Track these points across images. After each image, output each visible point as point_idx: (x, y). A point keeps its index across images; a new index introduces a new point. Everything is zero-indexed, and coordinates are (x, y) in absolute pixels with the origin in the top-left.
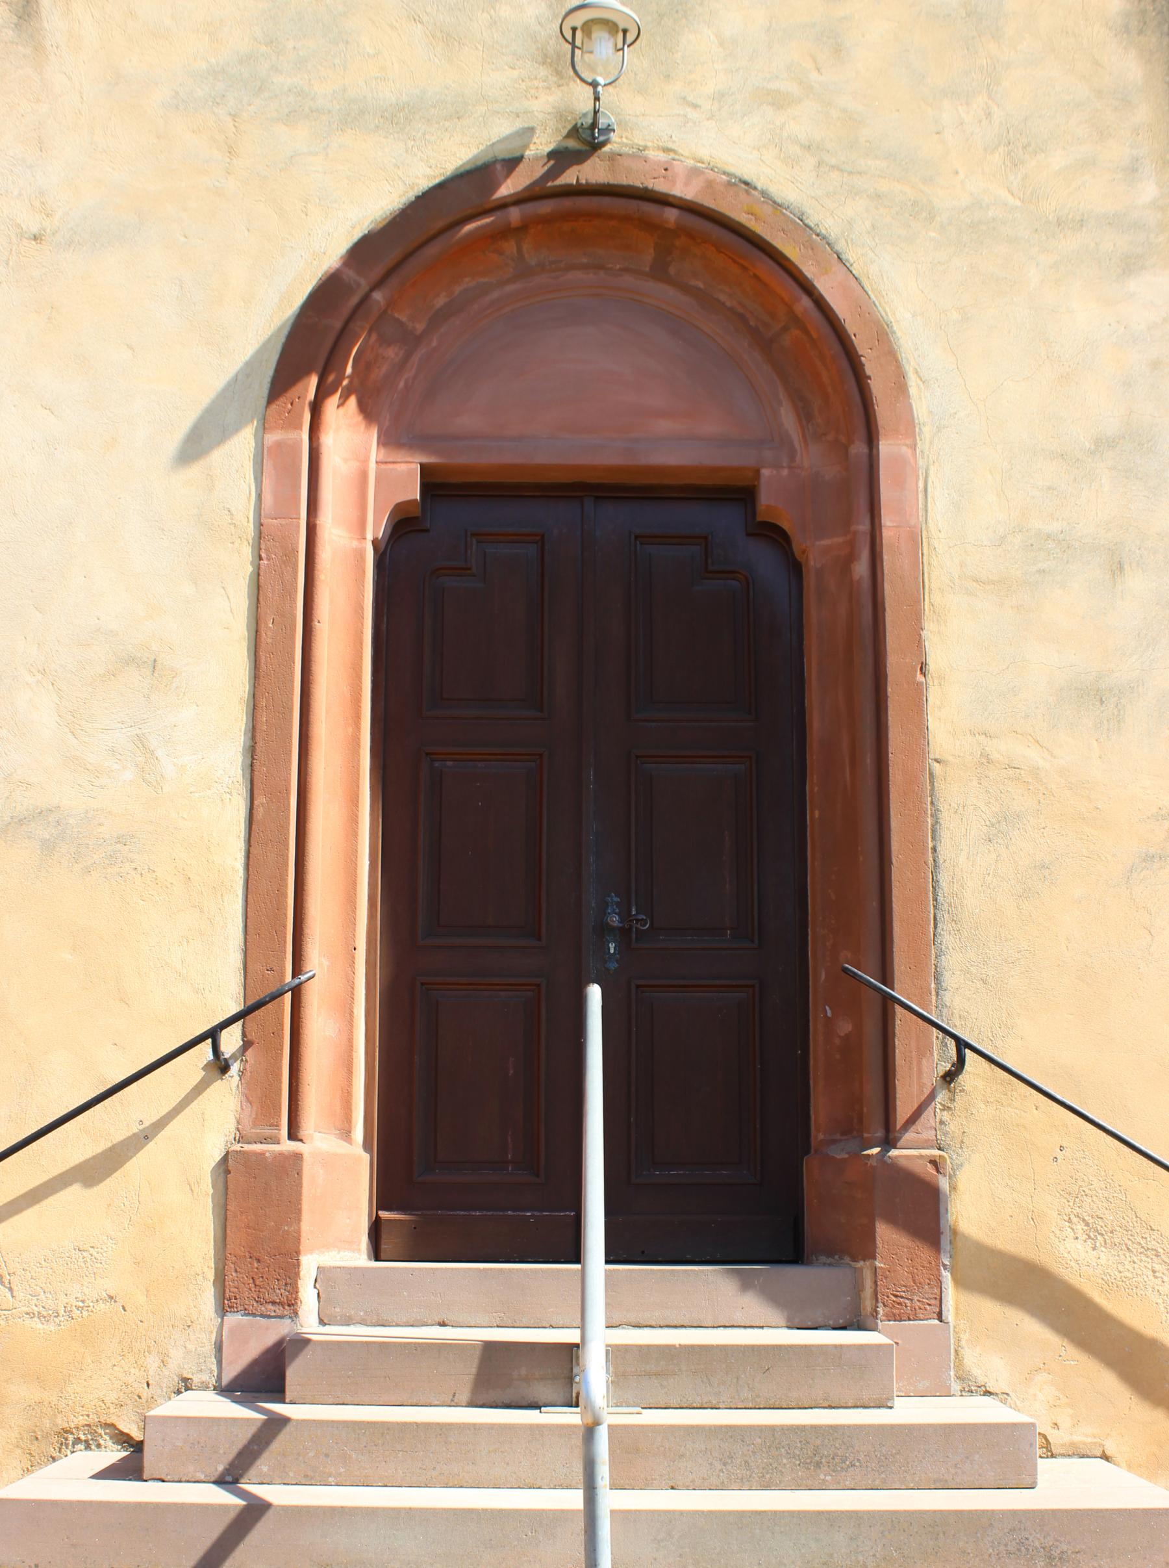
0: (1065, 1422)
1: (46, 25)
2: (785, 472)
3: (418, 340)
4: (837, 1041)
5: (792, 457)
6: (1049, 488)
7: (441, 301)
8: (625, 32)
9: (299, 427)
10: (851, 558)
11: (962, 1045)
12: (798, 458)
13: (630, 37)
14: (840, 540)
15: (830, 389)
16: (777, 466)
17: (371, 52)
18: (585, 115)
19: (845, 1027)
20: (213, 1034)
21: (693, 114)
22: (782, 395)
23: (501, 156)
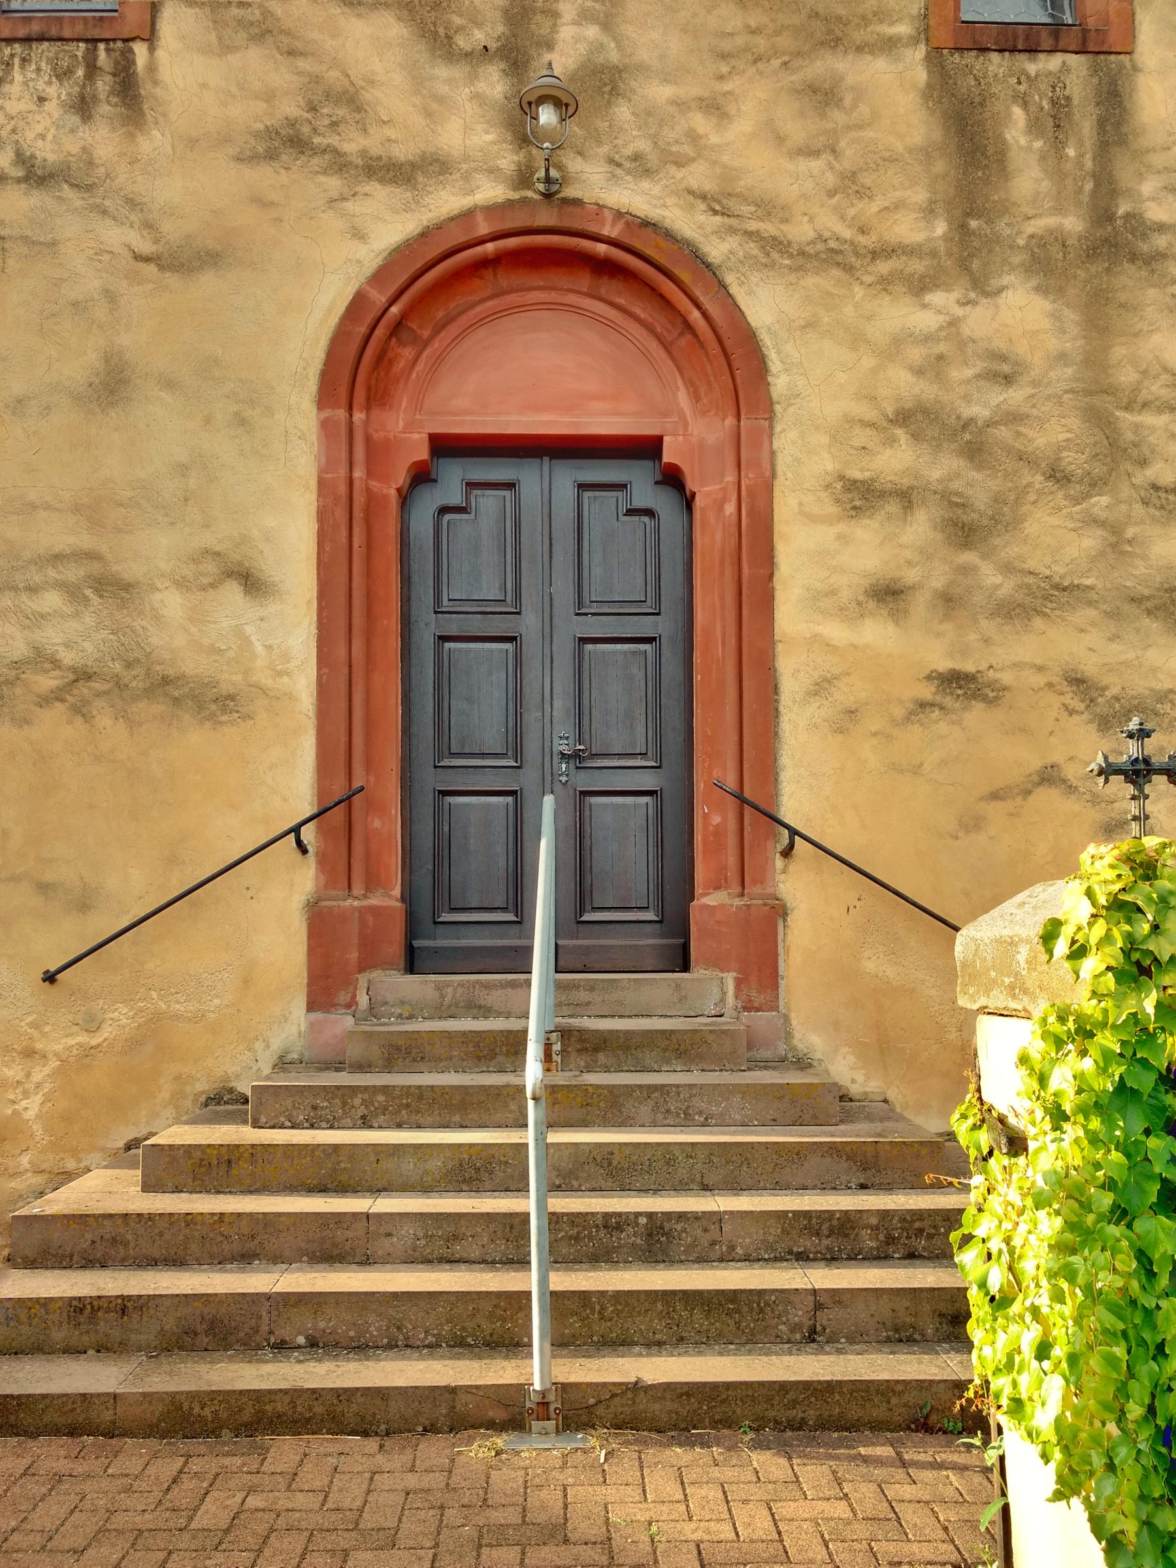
0: (860, 1078)
1: (143, 92)
2: (681, 438)
3: (426, 343)
4: (711, 828)
5: (686, 429)
6: (864, 448)
7: (440, 314)
8: (567, 105)
9: (747, 486)
10: (724, 501)
11: (794, 832)
12: (690, 429)
13: (571, 110)
14: (718, 487)
15: (712, 378)
16: (675, 434)
17: (386, 119)
18: (558, 1517)
19: (716, 819)
20: (296, 830)
21: (619, 171)
22: (680, 383)
23: (480, 204)
